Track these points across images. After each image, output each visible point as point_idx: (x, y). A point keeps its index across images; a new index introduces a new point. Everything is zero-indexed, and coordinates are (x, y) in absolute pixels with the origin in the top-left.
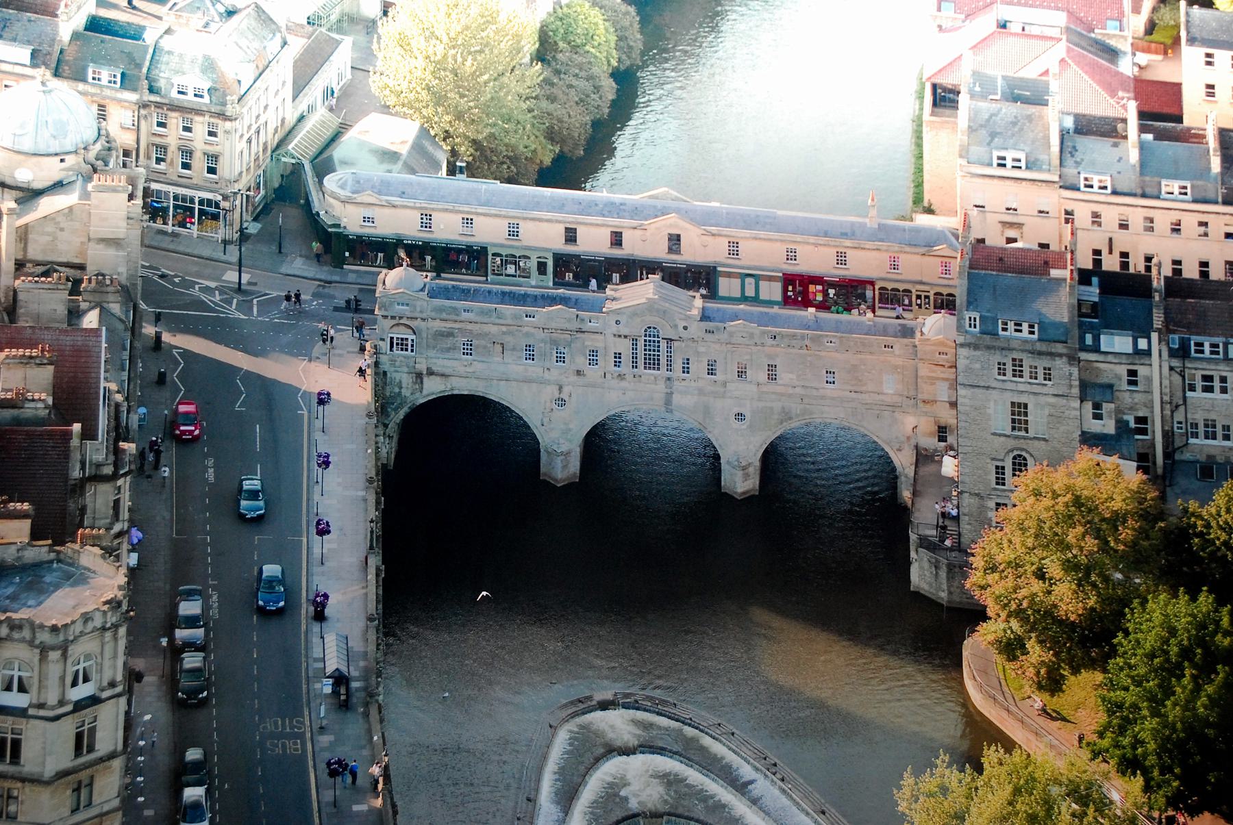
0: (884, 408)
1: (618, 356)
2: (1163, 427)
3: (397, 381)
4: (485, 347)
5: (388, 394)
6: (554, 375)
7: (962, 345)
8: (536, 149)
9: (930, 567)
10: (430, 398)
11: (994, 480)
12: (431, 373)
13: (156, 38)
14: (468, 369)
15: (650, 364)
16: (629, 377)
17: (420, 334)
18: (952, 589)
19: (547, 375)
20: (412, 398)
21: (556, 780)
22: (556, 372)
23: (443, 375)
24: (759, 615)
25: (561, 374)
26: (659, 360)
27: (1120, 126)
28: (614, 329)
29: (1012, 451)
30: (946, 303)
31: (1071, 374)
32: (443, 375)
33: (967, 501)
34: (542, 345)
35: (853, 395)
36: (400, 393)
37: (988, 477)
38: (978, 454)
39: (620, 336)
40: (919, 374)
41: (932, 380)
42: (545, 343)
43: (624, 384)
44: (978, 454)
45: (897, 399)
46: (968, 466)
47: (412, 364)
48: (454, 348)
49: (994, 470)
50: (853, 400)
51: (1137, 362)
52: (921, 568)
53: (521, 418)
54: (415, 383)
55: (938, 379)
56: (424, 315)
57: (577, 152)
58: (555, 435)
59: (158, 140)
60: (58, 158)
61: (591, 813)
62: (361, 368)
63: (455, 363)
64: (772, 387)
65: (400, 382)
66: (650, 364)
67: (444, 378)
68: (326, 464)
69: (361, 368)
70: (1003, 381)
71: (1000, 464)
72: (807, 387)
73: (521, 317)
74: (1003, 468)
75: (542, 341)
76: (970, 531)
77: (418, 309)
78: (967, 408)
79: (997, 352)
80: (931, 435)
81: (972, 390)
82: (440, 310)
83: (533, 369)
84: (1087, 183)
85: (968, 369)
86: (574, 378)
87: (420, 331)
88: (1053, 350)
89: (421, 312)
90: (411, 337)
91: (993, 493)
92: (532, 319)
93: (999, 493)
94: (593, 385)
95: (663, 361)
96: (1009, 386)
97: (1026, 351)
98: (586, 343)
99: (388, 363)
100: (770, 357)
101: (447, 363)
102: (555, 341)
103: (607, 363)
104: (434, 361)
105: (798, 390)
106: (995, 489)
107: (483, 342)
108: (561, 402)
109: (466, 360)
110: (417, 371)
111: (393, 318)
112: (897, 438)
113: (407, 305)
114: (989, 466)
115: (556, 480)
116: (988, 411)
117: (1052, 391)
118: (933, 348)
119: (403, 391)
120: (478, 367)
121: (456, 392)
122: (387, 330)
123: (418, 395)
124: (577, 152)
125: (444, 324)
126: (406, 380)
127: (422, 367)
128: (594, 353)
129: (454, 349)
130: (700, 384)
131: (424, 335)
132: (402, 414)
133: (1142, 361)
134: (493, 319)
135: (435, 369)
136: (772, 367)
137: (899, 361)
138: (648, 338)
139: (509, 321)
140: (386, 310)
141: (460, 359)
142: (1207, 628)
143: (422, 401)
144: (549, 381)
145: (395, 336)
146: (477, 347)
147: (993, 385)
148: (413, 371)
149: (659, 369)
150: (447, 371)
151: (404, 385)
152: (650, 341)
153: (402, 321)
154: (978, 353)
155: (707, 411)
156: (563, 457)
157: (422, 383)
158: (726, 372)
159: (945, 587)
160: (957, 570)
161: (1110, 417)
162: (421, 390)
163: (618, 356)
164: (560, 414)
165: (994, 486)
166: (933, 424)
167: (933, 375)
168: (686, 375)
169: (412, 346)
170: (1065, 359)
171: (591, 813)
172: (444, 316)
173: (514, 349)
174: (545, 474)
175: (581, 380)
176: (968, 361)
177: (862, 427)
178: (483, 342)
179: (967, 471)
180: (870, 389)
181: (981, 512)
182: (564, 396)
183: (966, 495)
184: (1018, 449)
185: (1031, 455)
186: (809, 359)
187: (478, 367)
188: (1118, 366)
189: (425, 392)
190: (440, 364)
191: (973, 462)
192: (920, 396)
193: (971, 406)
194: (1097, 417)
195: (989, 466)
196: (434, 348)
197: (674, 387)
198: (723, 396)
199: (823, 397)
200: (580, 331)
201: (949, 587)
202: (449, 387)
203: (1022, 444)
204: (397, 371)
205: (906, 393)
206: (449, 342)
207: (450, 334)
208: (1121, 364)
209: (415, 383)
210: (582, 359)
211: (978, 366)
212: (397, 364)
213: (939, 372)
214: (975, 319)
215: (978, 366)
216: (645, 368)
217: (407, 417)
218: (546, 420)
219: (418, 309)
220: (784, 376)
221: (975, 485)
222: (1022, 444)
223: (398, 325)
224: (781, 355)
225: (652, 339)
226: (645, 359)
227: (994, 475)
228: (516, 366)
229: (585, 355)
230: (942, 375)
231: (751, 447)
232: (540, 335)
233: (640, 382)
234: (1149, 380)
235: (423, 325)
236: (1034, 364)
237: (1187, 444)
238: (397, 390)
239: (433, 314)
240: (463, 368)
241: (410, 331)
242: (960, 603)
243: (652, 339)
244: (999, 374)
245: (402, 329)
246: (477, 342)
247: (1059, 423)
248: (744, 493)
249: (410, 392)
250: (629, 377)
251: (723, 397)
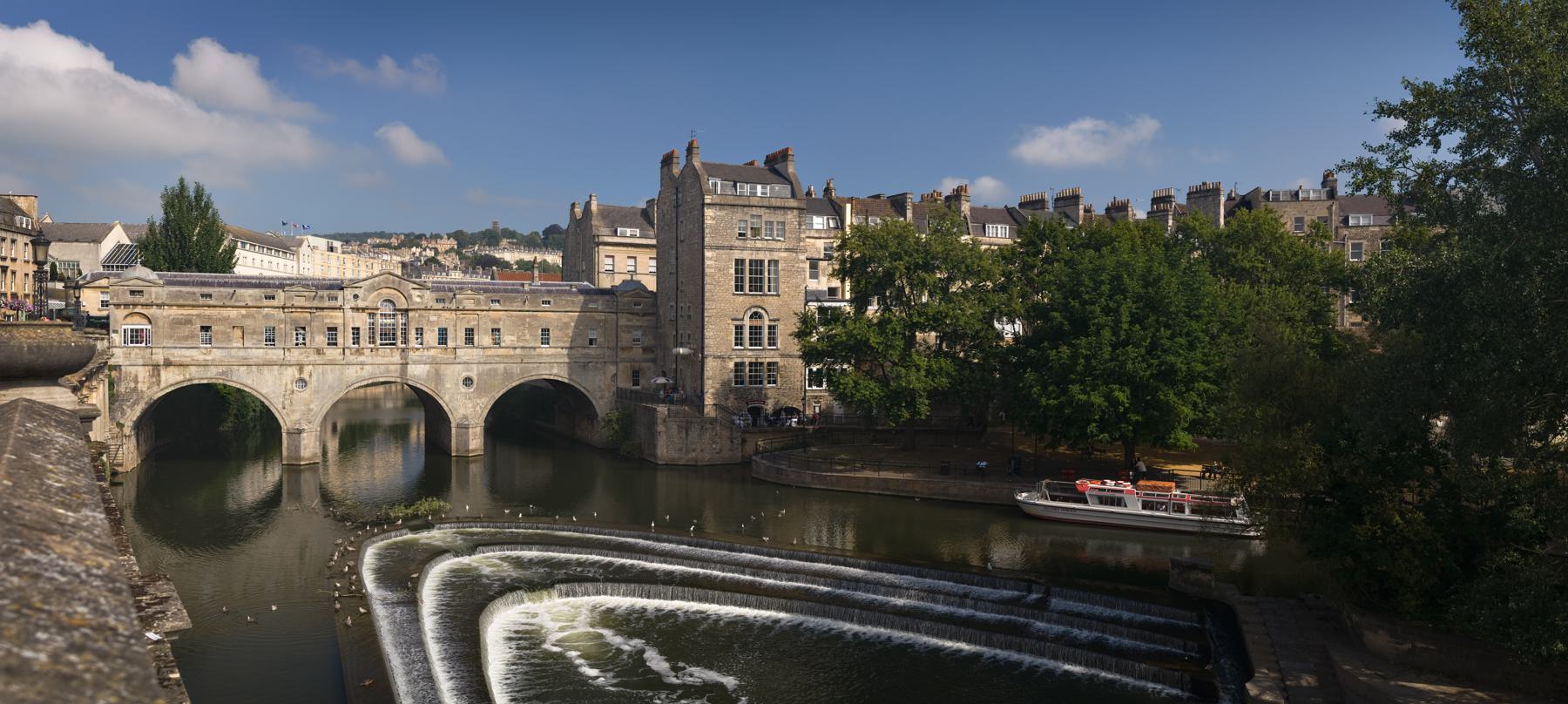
1: (356, 330)
4: (224, 333)
5: (123, 390)
9: (679, 432)
16: (367, 352)
17: (156, 323)
20: (149, 393)
22: (295, 355)
23: (180, 365)
29: (750, 309)
32: (180, 365)
40: (620, 324)
41: (629, 329)
43: (362, 358)
46: (713, 329)
48: (193, 336)
55: (633, 327)
63: (194, 353)
65: (136, 376)
68: (468, 381)
71: (738, 323)
72: (526, 348)
75: (281, 321)
85: (715, 230)
86: (314, 357)
91: (734, 353)
94: (332, 363)
97: (764, 207)
100: (495, 321)
101: (185, 352)
104: (173, 351)
107: (222, 328)
110: (155, 363)
112: (599, 387)
119: (140, 385)
123: (155, 388)
126: (143, 373)
127: (159, 357)
128: (333, 330)
131: (161, 324)
135: (172, 359)
147: (736, 244)
148: (151, 363)
150: (187, 361)
151: (140, 379)
154: (722, 213)
155: (438, 377)
157: (159, 375)
158: (456, 338)
163: (356, 330)
164: (305, 394)
173: (254, 333)
178: (222, 328)
179: (711, 334)
182: (305, 376)
185: (766, 312)
186: (528, 320)
189: (163, 385)
190: (178, 355)
202: (188, 377)
206: (186, 330)
208: (820, 238)
209: (152, 376)
218: (287, 402)
220: (508, 339)
222: (758, 301)
229: (324, 333)
230: (638, 324)
232: (280, 314)
238: (132, 385)
241: (145, 321)
245: (137, 319)
250: (367, 352)
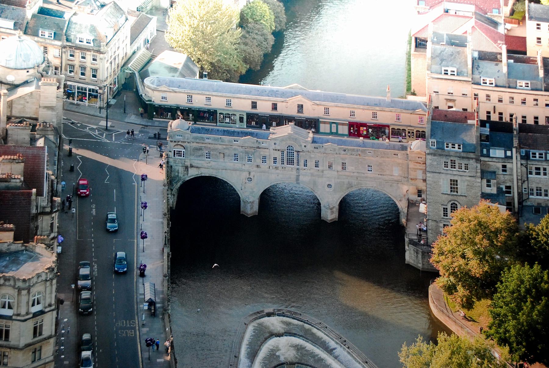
0: (393, 182)
1: (275, 159)
2: (518, 190)
3: (177, 170)
4: (216, 155)
5: (173, 176)
6: (247, 167)
7: (428, 154)
8: (238, 66)
9: (414, 253)
10: (192, 178)
11: (443, 214)
12: (192, 166)
13: (69, 17)
14: (209, 165)
15: (289, 162)
16: (280, 168)
17: (187, 149)
18: (424, 263)
19: (243, 167)
20: (183, 178)
21: (248, 348)
22: (247, 166)
23: (197, 167)
24: (338, 274)
25: (250, 167)
26: (293, 161)
27: (499, 56)
28: (273, 147)
29: (451, 201)
30: (421, 135)
31: (477, 167)
32: (197, 167)
33: (430, 223)
34: (241, 154)
35: (380, 176)
36: (178, 175)
37: (440, 213)
38: (436, 203)
39: (276, 150)
40: (409, 167)
41: (415, 170)
42: (243, 153)
43: (278, 171)
44: (436, 203)
45: (399, 178)
46: (431, 208)
47: (183, 162)
48: (202, 155)
49: (443, 210)
50: (380, 178)
51: (506, 161)
52: (410, 253)
53: (232, 187)
54: (185, 171)
55: (417, 169)
56: (189, 141)
57: (257, 68)
58: (247, 194)
59: (70, 63)
60: (26, 71)
61: (263, 363)
62: (161, 164)
63: (203, 162)
64: (344, 173)
65: (178, 170)
66: (289, 162)
67: (197, 169)
69: (161, 164)
70: (447, 170)
71: (445, 207)
72: (359, 173)
73: (232, 142)
74: (447, 209)
75: (242, 152)
76: (432, 237)
77: (186, 138)
78: (431, 182)
79: (444, 157)
80: (414, 194)
81: (433, 174)
82: (196, 138)
83: (238, 165)
84: (484, 82)
85: (431, 165)
86: (256, 169)
87: (187, 148)
88: (469, 156)
89: (187, 139)
90: (183, 150)
91: (442, 220)
92: (237, 142)
93: (445, 220)
94: (264, 172)
95: (295, 161)
96: (449, 172)
97: (457, 156)
98: (261, 153)
99: (173, 162)
100: (343, 159)
101: (199, 162)
102: (247, 152)
103: (270, 162)
104: (193, 161)
105: (355, 174)
106: (443, 218)
107: (215, 153)
108: (250, 179)
109: (208, 161)
110: (186, 165)
111: (175, 142)
112: (399, 195)
113: (181, 136)
114: (441, 208)
115: (248, 214)
116: (440, 183)
117: (469, 174)
118: (415, 155)
119: (180, 174)
120: (213, 164)
121: (203, 175)
122: (172, 147)
123: (186, 176)
124: (257, 68)
125: (197, 145)
126: (181, 169)
127: (188, 164)
128: (264, 157)
129: (202, 156)
130: (312, 171)
131: (189, 150)
132: (179, 185)
133: (509, 161)
134: (220, 142)
135: (194, 164)
136: (344, 164)
137: (400, 161)
138: (288, 151)
139: (227, 143)
140: (172, 138)
141: (205, 160)
142: (538, 280)
143: (188, 179)
144: (244, 170)
145: (176, 150)
146: (213, 155)
147: (442, 172)
148: (184, 165)
149: (293, 165)
150: (199, 166)
151: (180, 172)
152: (289, 152)
153: (179, 143)
154: (435, 157)
155: (315, 183)
156: (251, 204)
157: (188, 171)
158: (323, 166)
159: (421, 262)
160: (426, 254)
161: (494, 186)
162: (188, 174)
163: (275, 159)
164: (250, 185)
165: (443, 217)
166: (415, 189)
167: (416, 167)
168: (305, 167)
169: (184, 154)
170: (474, 160)
171: (263, 363)
172: (198, 141)
173: (229, 156)
174: (243, 212)
175: (259, 170)
176: (431, 161)
177: (384, 190)
178: (215, 153)
179: (431, 210)
180: (387, 174)
181: (437, 229)
182: (251, 177)
183: (430, 221)
184: (453, 200)
185: (459, 203)
186: (360, 160)
187: (213, 164)
188: (498, 163)
189: (189, 175)
190: (196, 162)
191: (433, 206)
192: (410, 177)
193: (433, 181)
194: (489, 186)
195: (441, 208)
196: (193, 155)
197: (300, 173)
198: (322, 177)
199: (366, 177)
200: (258, 148)
201: (422, 262)
202: (200, 172)
203: (455, 198)
204: (177, 166)
205: (403, 175)
206: (200, 152)
207: (200, 149)
208: (499, 162)
209: (185, 171)
210: (259, 160)
211: (435, 163)
212: (177, 162)
213: (418, 166)
214: (434, 142)
215: (435, 163)
216: (287, 164)
217: (181, 186)
218: (243, 188)
219: (186, 138)
220: (349, 168)
221: (434, 216)
222: (455, 198)
223: (177, 145)
224: (348, 158)
225: (290, 151)
226: (287, 160)
227: (443, 212)
228: (230, 163)
229: (260, 158)
230: (420, 167)
231: (334, 199)
232: (241, 149)
233: (285, 170)
234: (512, 169)
235: (188, 145)
236: (460, 162)
237: (529, 198)
238: (177, 174)
239: (193, 140)
240: (206, 164)
241: (183, 148)
242: (428, 269)
243: (290, 151)
244: (445, 167)
245: (179, 147)
246: (212, 153)
247: (471, 188)
248: (331, 220)
249: (182, 175)
250: (280, 168)
251: (322, 177)
